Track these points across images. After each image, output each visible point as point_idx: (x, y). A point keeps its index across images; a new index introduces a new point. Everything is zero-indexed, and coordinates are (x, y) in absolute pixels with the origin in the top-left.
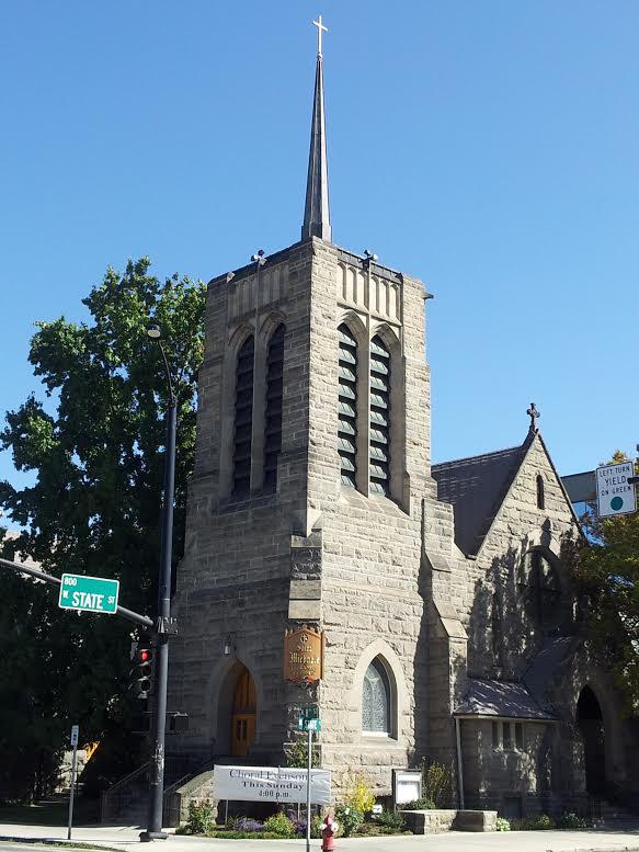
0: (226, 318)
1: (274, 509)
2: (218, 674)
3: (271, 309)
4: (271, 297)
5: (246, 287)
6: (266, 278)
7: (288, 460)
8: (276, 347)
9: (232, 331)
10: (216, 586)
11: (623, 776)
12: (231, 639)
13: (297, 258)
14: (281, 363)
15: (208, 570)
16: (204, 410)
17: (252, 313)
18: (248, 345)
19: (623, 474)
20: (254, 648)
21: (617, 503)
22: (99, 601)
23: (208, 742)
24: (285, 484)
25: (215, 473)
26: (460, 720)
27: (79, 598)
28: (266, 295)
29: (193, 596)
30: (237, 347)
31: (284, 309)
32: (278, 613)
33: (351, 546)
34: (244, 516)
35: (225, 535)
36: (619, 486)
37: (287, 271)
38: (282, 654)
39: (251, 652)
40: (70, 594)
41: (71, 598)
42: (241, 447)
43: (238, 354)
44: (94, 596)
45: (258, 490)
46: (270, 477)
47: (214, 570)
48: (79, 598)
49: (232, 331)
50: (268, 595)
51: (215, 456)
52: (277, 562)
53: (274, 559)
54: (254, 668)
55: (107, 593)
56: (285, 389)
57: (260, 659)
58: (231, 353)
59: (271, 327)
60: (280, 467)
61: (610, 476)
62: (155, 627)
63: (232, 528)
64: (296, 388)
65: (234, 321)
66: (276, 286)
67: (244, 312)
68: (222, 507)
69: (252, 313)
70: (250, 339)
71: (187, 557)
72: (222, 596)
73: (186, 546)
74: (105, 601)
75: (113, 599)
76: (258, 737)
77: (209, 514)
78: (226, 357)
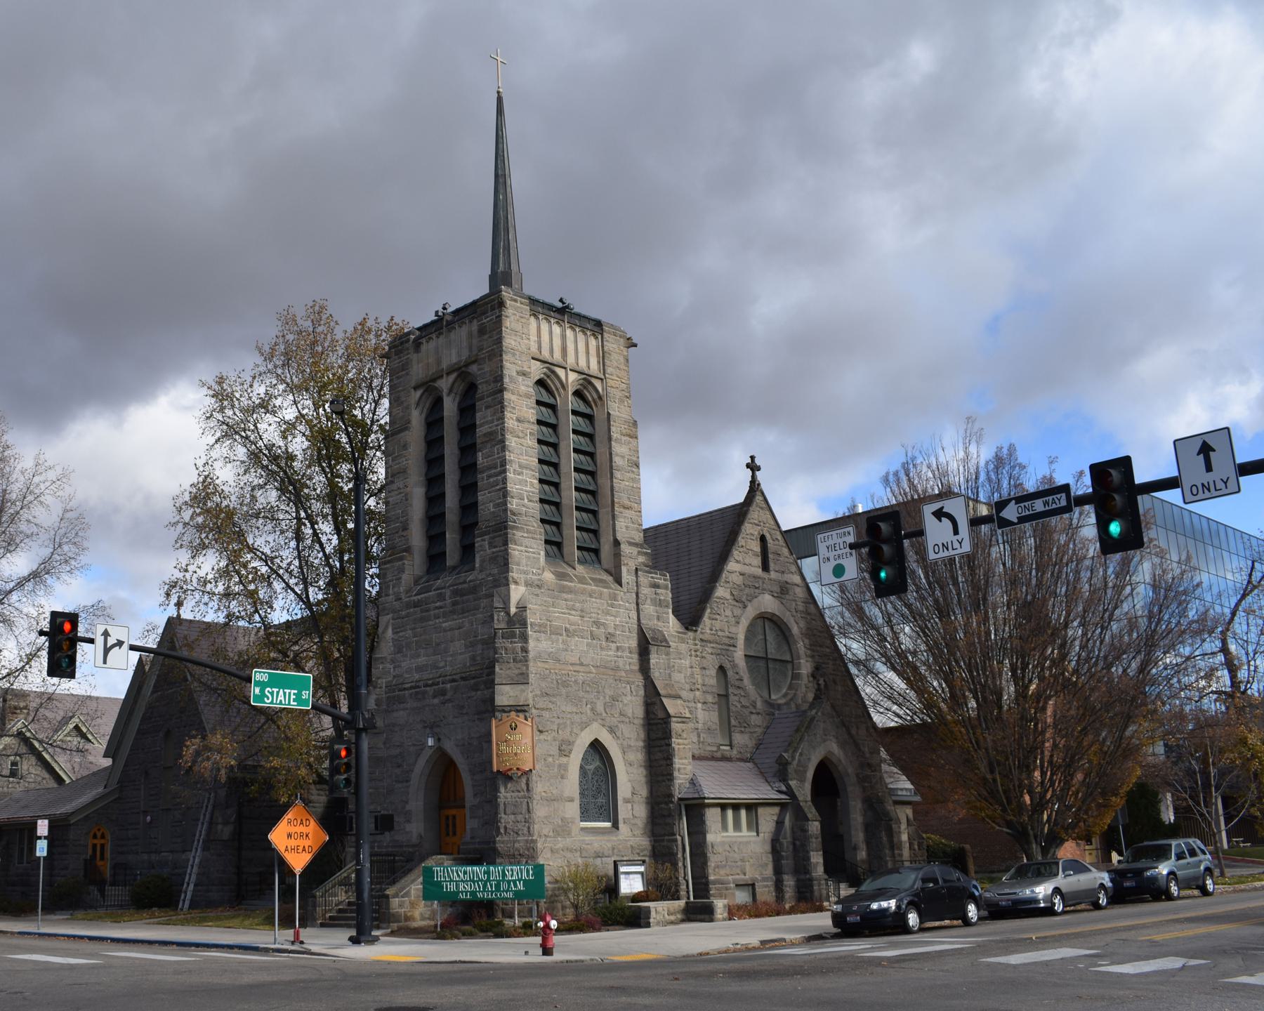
3: (461, 371)
5: (432, 344)
12: (432, 727)
13: (484, 313)
23: (415, 840)
27: (272, 694)
35: (422, 619)
36: (840, 552)
37: (475, 326)
40: (262, 691)
41: (262, 697)
42: (434, 519)
44: (287, 691)
45: (454, 568)
46: (468, 550)
48: (272, 694)
61: (831, 542)
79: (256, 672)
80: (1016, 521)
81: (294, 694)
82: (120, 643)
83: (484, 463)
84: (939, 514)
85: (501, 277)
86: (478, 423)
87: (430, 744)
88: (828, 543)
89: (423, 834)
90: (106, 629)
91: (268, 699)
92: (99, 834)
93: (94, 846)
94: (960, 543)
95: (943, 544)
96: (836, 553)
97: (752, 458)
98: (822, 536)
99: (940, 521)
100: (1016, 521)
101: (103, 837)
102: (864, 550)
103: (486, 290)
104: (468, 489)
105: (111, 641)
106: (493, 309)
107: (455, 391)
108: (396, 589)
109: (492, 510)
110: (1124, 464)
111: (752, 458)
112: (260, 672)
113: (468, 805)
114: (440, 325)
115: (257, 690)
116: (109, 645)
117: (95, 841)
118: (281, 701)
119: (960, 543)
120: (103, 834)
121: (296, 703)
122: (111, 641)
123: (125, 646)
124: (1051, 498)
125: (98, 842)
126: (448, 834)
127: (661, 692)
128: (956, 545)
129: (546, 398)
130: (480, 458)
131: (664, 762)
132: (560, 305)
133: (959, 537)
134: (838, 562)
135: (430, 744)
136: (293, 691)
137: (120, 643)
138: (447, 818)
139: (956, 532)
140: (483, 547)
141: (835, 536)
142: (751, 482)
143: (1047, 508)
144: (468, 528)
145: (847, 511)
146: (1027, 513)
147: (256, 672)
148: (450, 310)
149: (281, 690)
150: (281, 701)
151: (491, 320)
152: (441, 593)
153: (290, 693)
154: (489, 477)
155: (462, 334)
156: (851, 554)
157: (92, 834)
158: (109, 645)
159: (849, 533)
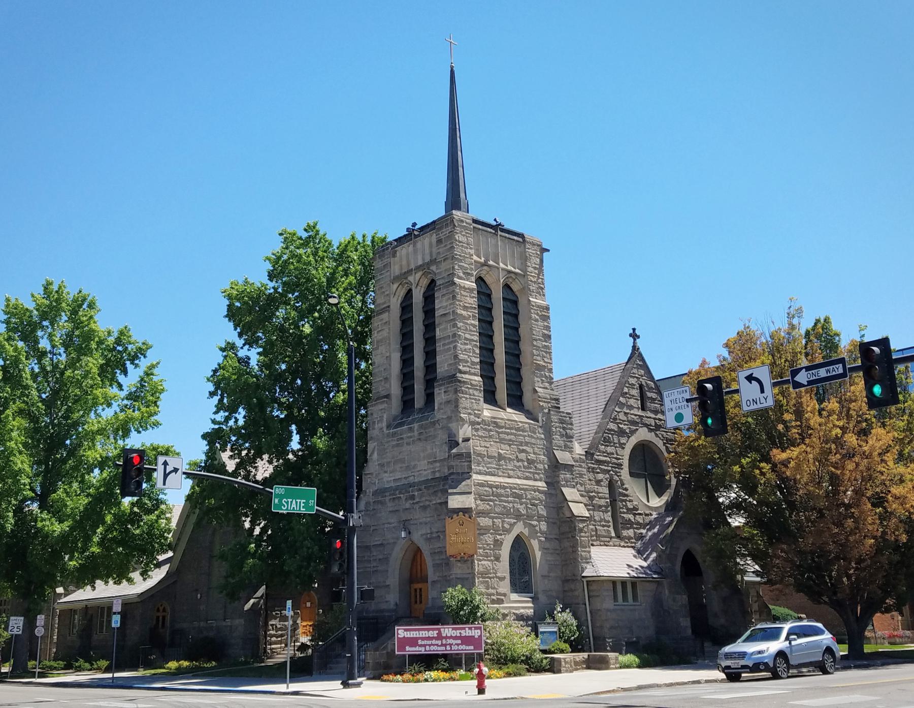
0: (390, 277)
1: (434, 423)
2: (397, 554)
3: (424, 267)
4: (423, 259)
5: (404, 252)
6: (419, 245)
7: (441, 385)
8: (429, 298)
9: (395, 286)
10: (392, 484)
11: (722, 621)
12: (405, 525)
13: (441, 228)
14: (433, 310)
15: (386, 472)
16: (377, 348)
17: (410, 272)
18: (409, 295)
19: (682, 395)
20: (424, 532)
21: (679, 418)
22: (302, 505)
23: (392, 606)
24: (441, 404)
25: (388, 396)
26: (587, 581)
27: (287, 503)
28: (420, 258)
29: (375, 493)
30: (400, 298)
31: (433, 268)
32: (440, 504)
33: (494, 450)
34: (411, 430)
35: (398, 445)
36: (679, 404)
37: (434, 238)
38: (445, 536)
39: (422, 535)
40: (280, 501)
41: (280, 505)
42: (407, 376)
43: (401, 304)
44: (298, 501)
45: (420, 409)
46: (430, 397)
47: (391, 472)
48: (287, 503)
49: (395, 286)
50: (431, 491)
51: (387, 385)
52: (438, 464)
53: (435, 461)
54: (426, 549)
55: (307, 498)
56: (437, 330)
57: (429, 540)
58: (395, 304)
59: (425, 282)
60: (436, 391)
61: (673, 397)
62: (346, 521)
63: (402, 439)
64: (446, 329)
65: (396, 279)
66: (427, 251)
67: (403, 271)
68: (396, 423)
69: (410, 272)
70: (410, 292)
71: (370, 464)
72: (397, 492)
73: (369, 454)
74: (306, 504)
75: (313, 502)
76: (430, 601)
77: (385, 429)
78: (391, 307)
79: (276, 488)
80: (806, 384)
81: (303, 503)
82: (176, 470)
83: (440, 335)
84: (750, 378)
85: (454, 199)
86: (436, 307)
87: (403, 536)
88: (671, 398)
89: (398, 602)
90: (166, 461)
91: (284, 507)
92: (161, 609)
93: (158, 617)
94: (766, 399)
95: (753, 400)
96: (677, 405)
97: (634, 330)
98: (667, 393)
99: (751, 383)
100: (806, 384)
101: (164, 610)
102: (696, 403)
103: (443, 213)
104: (430, 354)
105: (169, 469)
106: (447, 225)
107: (420, 285)
108: (380, 425)
109: (446, 369)
110: (884, 343)
111: (634, 330)
112: (279, 488)
113: (429, 581)
114: (411, 236)
115: (277, 501)
116: (167, 472)
117: (159, 614)
118: (294, 508)
119: (766, 399)
120: (164, 608)
121: (304, 510)
122: (169, 469)
123: (179, 472)
124: (831, 367)
125: (160, 614)
126: (416, 602)
127: (568, 498)
128: (763, 400)
129: (484, 290)
130: (438, 333)
131: (571, 550)
132: (494, 223)
133: (764, 395)
134: (679, 411)
135: (403, 536)
136: (303, 501)
137: (176, 470)
138: (416, 590)
139: (762, 391)
140: (440, 396)
141: (676, 393)
142: (633, 347)
143: (829, 375)
144: (430, 382)
145: (725, 353)
146: (814, 378)
147: (276, 488)
148: (417, 227)
149: (294, 500)
150: (294, 508)
151: (445, 235)
152: (411, 427)
153: (300, 502)
154: (444, 345)
155: (426, 242)
156: (688, 406)
157: (156, 609)
158: (167, 472)
159: (686, 391)
